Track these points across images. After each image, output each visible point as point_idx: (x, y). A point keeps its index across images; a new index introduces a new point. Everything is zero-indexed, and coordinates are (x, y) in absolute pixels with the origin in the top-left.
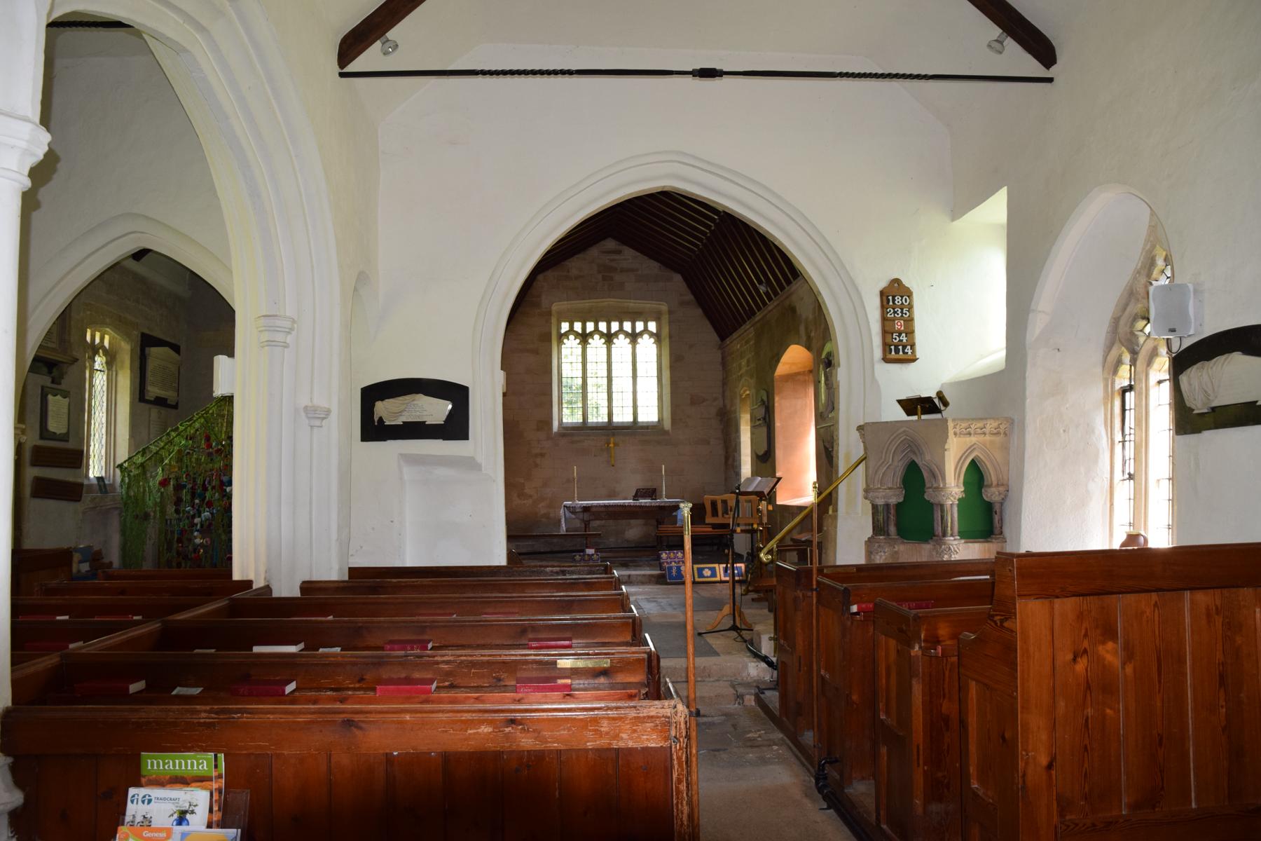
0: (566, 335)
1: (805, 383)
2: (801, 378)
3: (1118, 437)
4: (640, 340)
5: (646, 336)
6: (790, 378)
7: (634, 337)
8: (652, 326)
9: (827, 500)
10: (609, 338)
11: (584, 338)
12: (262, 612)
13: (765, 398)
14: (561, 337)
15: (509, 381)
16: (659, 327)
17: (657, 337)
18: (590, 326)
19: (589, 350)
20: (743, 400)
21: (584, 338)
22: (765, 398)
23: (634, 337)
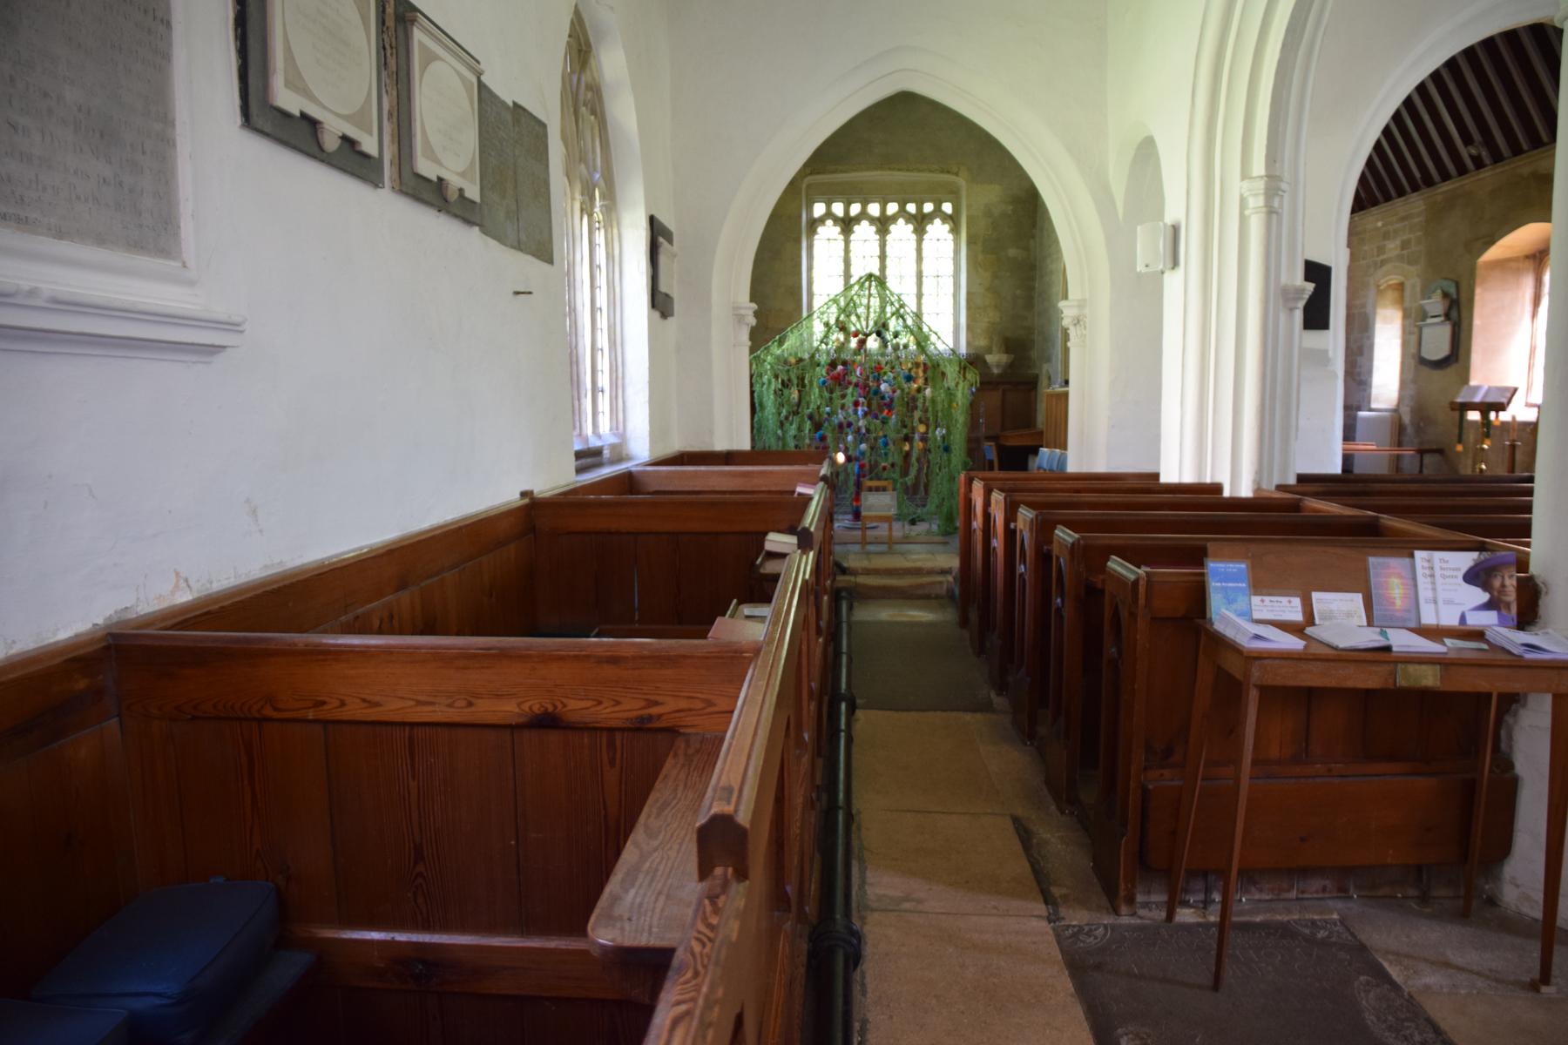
0: (822, 220)
1: (1518, 272)
2: (1513, 265)
3: (804, 648)
4: (892, 228)
5: (865, 223)
6: (1501, 264)
7: (920, 223)
8: (947, 208)
9: (969, 482)
10: (883, 225)
11: (847, 224)
12: (753, 447)
13: (1452, 290)
14: (814, 224)
15: (1352, 255)
16: (956, 209)
17: (953, 220)
18: (855, 209)
19: (925, 244)
20: (1380, 292)
21: (847, 224)
22: (1452, 290)
23: (920, 223)
